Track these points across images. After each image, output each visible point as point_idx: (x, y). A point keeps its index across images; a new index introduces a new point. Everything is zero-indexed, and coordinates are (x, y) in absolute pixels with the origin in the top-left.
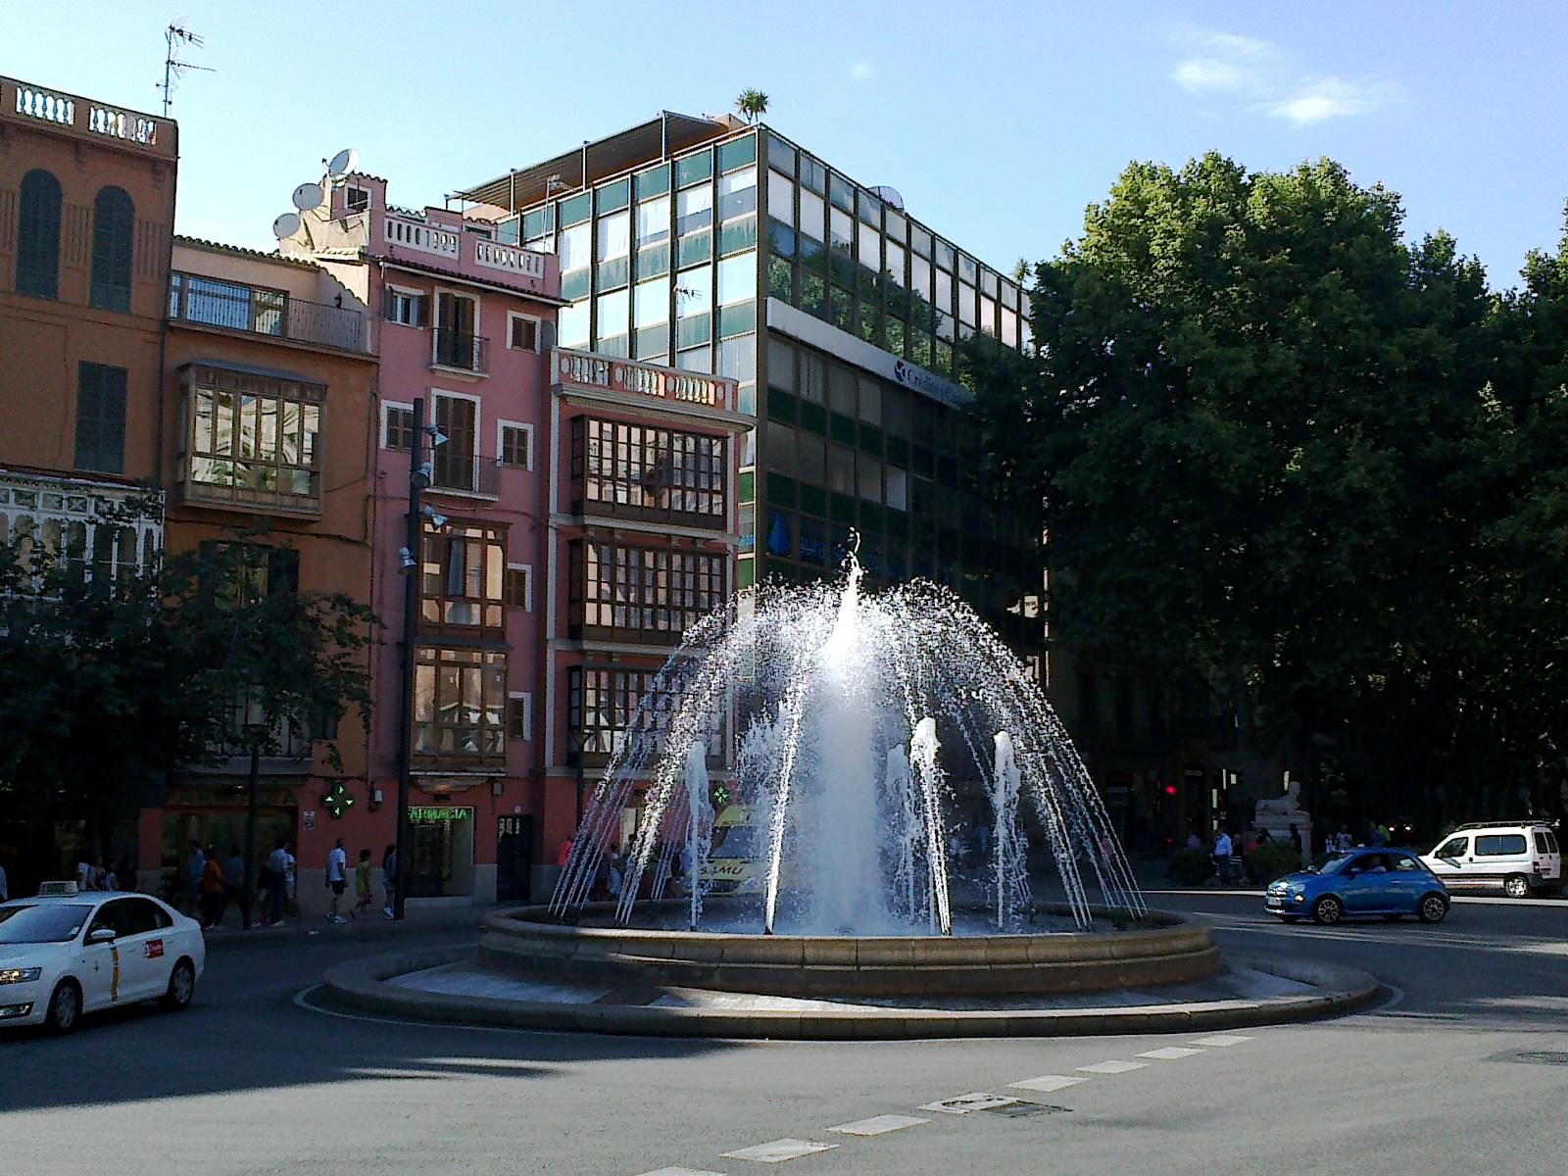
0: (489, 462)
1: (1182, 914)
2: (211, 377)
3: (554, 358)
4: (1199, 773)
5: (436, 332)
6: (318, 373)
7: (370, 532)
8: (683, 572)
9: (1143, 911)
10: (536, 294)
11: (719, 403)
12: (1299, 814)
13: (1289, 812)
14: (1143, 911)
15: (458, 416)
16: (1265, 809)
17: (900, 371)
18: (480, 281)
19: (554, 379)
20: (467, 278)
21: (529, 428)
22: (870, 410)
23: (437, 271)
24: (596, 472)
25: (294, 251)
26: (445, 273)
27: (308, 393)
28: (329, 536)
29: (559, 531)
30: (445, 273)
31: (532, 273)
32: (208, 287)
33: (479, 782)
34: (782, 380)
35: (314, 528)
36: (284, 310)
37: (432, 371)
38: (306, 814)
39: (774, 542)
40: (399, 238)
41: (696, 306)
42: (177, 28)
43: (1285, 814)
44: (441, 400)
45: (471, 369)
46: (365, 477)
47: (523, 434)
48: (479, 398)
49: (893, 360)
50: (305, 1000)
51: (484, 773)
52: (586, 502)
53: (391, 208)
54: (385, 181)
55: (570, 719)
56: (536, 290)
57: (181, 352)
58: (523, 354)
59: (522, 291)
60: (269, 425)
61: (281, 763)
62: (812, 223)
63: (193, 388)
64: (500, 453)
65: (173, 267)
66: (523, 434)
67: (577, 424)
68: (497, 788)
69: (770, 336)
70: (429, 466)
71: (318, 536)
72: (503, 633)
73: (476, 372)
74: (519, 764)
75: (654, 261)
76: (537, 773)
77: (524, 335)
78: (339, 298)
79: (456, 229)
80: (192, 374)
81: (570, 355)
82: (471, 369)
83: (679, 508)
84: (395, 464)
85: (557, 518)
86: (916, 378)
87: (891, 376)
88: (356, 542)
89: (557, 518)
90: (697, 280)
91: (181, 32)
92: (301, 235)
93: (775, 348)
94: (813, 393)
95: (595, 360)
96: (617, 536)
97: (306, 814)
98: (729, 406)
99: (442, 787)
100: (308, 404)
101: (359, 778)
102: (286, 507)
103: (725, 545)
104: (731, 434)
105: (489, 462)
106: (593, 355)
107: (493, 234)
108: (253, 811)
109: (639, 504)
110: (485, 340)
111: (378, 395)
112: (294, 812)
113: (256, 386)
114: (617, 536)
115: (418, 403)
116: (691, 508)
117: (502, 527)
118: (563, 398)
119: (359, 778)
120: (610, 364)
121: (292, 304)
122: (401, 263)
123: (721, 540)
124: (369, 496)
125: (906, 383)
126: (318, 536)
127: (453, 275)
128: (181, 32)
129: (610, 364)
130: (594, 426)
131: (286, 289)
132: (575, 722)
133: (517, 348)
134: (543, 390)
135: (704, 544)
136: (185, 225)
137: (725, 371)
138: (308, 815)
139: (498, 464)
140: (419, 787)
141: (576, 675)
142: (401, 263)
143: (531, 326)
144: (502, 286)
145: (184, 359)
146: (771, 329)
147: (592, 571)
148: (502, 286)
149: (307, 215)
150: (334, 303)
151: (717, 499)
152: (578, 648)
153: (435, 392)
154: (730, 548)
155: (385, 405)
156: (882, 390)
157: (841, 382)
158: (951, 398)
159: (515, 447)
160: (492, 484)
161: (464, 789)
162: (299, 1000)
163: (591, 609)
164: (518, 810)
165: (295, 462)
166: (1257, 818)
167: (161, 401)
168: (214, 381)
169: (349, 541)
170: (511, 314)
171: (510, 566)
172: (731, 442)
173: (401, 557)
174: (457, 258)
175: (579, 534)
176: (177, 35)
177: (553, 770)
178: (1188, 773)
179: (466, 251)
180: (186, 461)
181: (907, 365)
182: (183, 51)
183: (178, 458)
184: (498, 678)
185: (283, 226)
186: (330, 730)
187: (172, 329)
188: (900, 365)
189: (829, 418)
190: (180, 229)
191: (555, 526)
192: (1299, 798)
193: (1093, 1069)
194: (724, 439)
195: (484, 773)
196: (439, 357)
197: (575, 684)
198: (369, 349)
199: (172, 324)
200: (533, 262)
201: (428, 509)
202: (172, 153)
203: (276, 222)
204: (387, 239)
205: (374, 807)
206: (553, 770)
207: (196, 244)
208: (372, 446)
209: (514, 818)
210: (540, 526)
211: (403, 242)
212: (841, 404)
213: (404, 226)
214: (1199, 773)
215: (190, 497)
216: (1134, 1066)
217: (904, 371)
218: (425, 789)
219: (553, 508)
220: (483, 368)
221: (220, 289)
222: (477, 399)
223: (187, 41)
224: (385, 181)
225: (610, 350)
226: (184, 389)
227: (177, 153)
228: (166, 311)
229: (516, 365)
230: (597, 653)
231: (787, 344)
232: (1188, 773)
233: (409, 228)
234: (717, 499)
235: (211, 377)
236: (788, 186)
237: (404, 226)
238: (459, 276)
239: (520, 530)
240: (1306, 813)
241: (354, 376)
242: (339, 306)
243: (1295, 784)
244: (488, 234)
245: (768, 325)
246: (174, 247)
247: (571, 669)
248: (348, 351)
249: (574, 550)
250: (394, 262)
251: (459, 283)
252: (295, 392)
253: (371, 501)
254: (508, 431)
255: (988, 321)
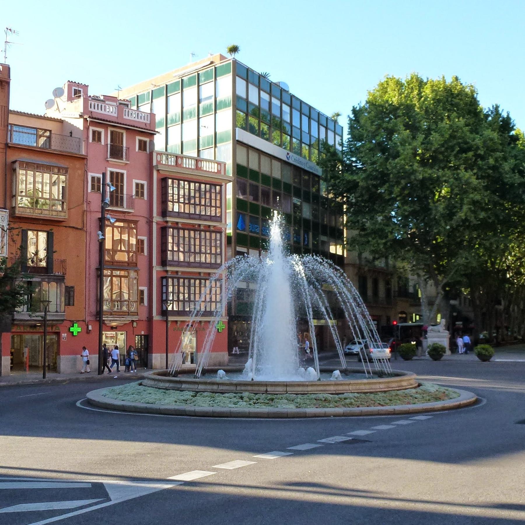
0: (130, 197)
1: (406, 372)
2: (25, 165)
3: (154, 155)
4: (404, 315)
5: (109, 146)
6: (63, 163)
7: (85, 226)
8: (216, 240)
9: (390, 371)
10: (147, 130)
11: (219, 172)
12: (445, 332)
13: (441, 331)
14: (390, 371)
15: (117, 178)
16: (431, 330)
17: (288, 156)
18: (126, 125)
19: (155, 163)
20: (121, 124)
21: (145, 183)
22: (277, 174)
23: (110, 122)
24: (177, 201)
25: (52, 113)
26: (113, 122)
27: (61, 170)
28: (70, 227)
29: (157, 223)
30: (113, 122)
31: (145, 121)
32: (21, 129)
33: (128, 322)
34: (242, 162)
35: (64, 224)
36: (49, 138)
37: (108, 161)
38: (63, 334)
39: (239, 226)
40: (98, 109)
41: (207, 133)
42: (9, 28)
43: (439, 332)
44: (112, 173)
45: (123, 160)
46: (83, 204)
47: (142, 186)
48: (126, 171)
49: (286, 151)
50: (81, 403)
51: (130, 318)
52: (167, 212)
53: (90, 96)
54: (88, 86)
55: (162, 297)
56: (147, 128)
57: (12, 156)
58: (143, 153)
59: (142, 128)
60: (30, 179)
61: (53, 315)
62: (254, 99)
63: (18, 169)
64: (134, 193)
65: (9, 122)
66: (142, 186)
67: (163, 181)
68: (135, 324)
69: (238, 143)
70: (108, 199)
71: (66, 227)
72: (136, 264)
73: (124, 161)
74: (144, 316)
75: (191, 114)
76: (150, 319)
77: (143, 146)
78: (71, 133)
79: (115, 104)
80: (17, 165)
81: (160, 154)
82: (123, 160)
83: (204, 214)
84: (95, 199)
85: (157, 218)
86: (295, 159)
87: (285, 159)
88: (80, 229)
89: (157, 218)
90: (207, 121)
91: (10, 30)
92: (55, 107)
93: (240, 148)
94: (254, 165)
95: (167, 155)
96: (180, 225)
97: (63, 334)
98: (223, 173)
99: (114, 324)
100: (61, 175)
101: (83, 321)
102: (53, 216)
103: (221, 228)
104: (223, 184)
105: (130, 197)
106: (166, 153)
107: (129, 106)
108: (45, 333)
109: (182, 211)
110: (128, 149)
111: (87, 171)
112: (58, 334)
113: (41, 168)
114: (180, 225)
115: (104, 175)
116: (209, 214)
117: (135, 222)
118: (158, 171)
119: (83, 321)
120: (176, 157)
121: (53, 136)
122: (95, 119)
123: (221, 226)
124: (85, 211)
125: (291, 161)
126: (66, 227)
127: (115, 123)
128: (10, 30)
129: (176, 157)
130: (170, 181)
131: (50, 129)
132: (164, 298)
133: (140, 151)
134: (150, 168)
135: (213, 228)
136: (13, 106)
137: (219, 159)
138: (64, 335)
139: (134, 197)
140: (105, 324)
141: (164, 280)
142: (95, 119)
143: (145, 142)
144: (134, 126)
145: (13, 159)
146: (238, 141)
147: (170, 240)
148: (134, 126)
149: (58, 99)
150: (69, 135)
151: (218, 210)
152: (165, 269)
153: (109, 169)
154: (223, 229)
155: (90, 175)
156: (281, 165)
157: (254, 156)
158: (308, 166)
159: (140, 190)
160: (131, 204)
161: (122, 325)
162: (78, 404)
163: (170, 204)
164: (143, 333)
165: (57, 198)
166: (428, 334)
167: (6, 175)
168: (26, 166)
169: (77, 229)
170: (138, 138)
171: (139, 237)
172: (223, 187)
173: (98, 235)
174: (116, 116)
175: (165, 224)
176: (9, 31)
177: (156, 317)
178: (400, 315)
179: (120, 112)
180: (16, 198)
181: (291, 154)
182: (11, 37)
183: (13, 197)
184: (135, 282)
185: (49, 104)
186: (71, 303)
187: (10, 147)
188: (288, 154)
189: (260, 175)
190: (12, 107)
191: (156, 221)
192: (445, 326)
193: (323, 441)
194: (221, 186)
195: (130, 318)
196: (110, 156)
197: (164, 284)
198: (84, 153)
199: (9, 145)
200: (146, 117)
201: (108, 216)
202: (7, 77)
203: (46, 103)
204: (90, 109)
205: (88, 332)
206: (156, 317)
207: (26, 115)
208: (85, 192)
209: (141, 336)
210: (150, 223)
211: (96, 110)
212: (265, 170)
213: (96, 104)
214: (404, 315)
215: (18, 213)
216: (323, 441)
217: (290, 156)
218: (108, 325)
219: (155, 214)
220: (127, 159)
221: (25, 130)
222: (125, 172)
223: (13, 33)
224: (88, 86)
225: (173, 151)
226: (15, 170)
227: (9, 77)
228: (6, 140)
229: (141, 157)
230: (172, 272)
231: (243, 146)
232: (400, 315)
233: (98, 105)
234: (218, 210)
235: (25, 165)
236: (244, 82)
237: (96, 104)
238: (118, 123)
239: (142, 223)
240: (447, 332)
241: (78, 164)
242: (71, 136)
243: (444, 320)
244: (127, 105)
245: (237, 139)
246: (9, 114)
247: (162, 278)
248: (76, 154)
249: (163, 231)
250: (92, 118)
251: (132, 129)
252: (56, 170)
253: (85, 213)
254: (137, 185)
255: (323, 136)
